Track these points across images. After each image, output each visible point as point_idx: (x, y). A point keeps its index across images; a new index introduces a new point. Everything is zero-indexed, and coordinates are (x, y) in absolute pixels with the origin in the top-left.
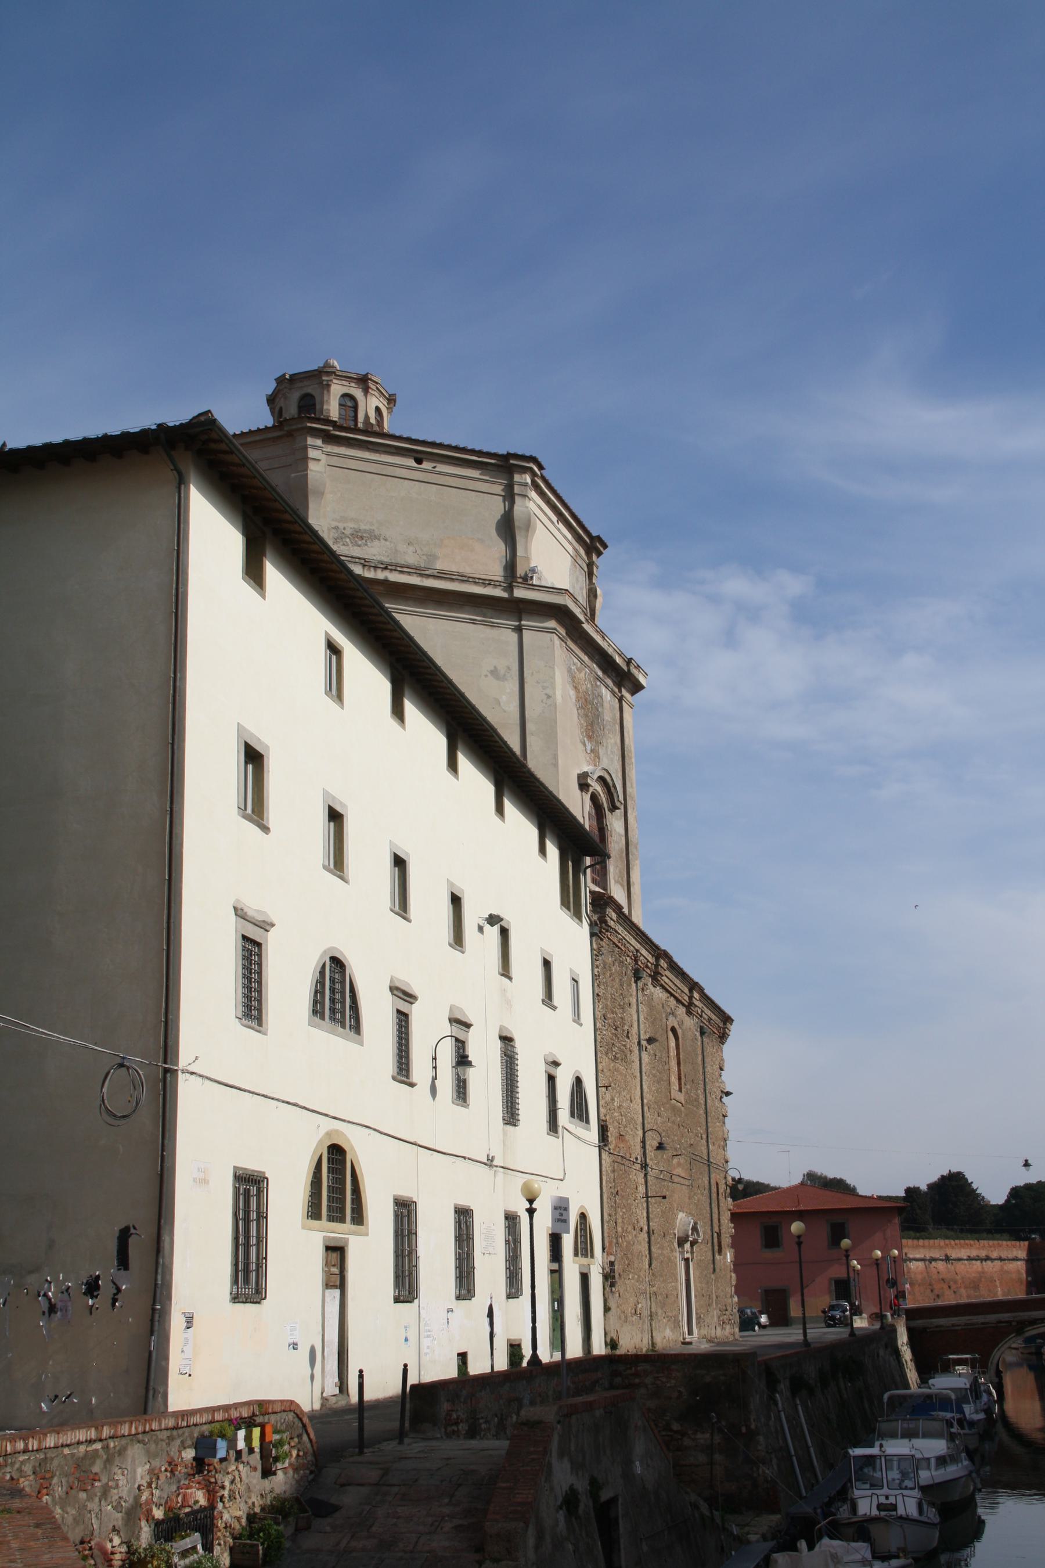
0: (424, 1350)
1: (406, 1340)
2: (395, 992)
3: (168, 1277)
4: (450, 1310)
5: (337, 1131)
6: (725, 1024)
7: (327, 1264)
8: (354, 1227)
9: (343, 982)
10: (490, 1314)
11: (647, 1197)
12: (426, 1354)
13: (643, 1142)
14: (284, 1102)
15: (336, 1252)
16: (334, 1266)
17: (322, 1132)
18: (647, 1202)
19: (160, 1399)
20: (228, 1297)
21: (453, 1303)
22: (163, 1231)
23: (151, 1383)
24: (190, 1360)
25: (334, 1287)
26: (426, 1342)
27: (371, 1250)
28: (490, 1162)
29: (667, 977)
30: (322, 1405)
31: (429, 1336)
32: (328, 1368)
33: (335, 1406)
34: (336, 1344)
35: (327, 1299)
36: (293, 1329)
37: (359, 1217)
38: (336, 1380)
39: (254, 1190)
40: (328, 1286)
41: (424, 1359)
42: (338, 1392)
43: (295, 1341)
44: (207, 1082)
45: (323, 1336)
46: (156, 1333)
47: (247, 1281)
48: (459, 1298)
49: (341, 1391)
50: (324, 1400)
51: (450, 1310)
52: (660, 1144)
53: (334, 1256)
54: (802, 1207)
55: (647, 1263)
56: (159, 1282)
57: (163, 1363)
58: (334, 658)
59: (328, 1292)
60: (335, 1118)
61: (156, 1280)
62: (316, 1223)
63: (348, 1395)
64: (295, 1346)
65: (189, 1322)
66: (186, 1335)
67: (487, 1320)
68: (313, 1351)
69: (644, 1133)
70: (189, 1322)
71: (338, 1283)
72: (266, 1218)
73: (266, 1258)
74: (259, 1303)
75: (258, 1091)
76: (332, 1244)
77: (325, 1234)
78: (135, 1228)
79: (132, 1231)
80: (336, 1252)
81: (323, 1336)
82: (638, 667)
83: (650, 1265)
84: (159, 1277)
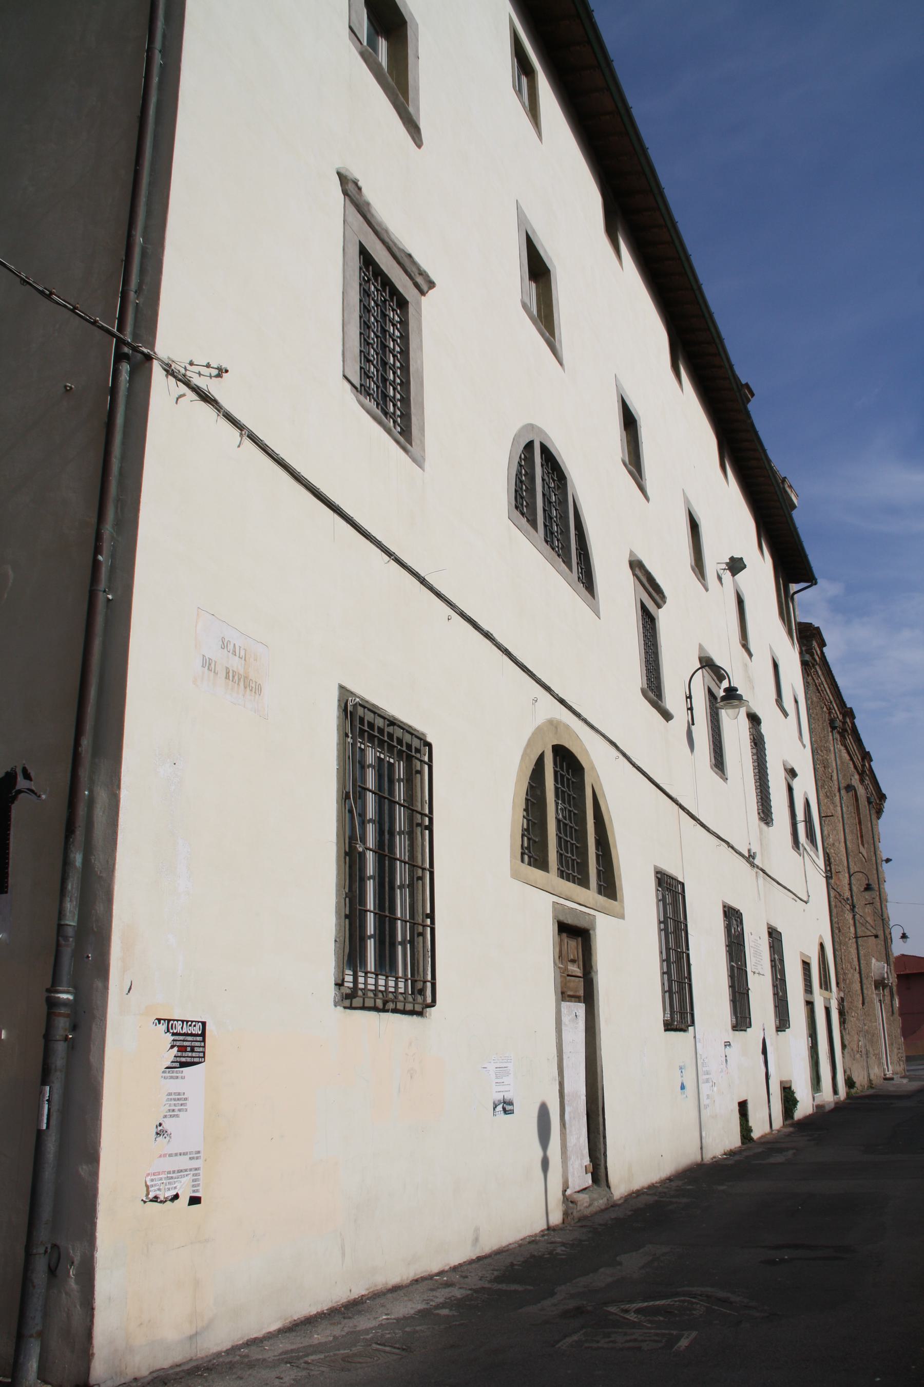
0: (704, 1101)
1: (683, 1087)
2: (638, 572)
3: (100, 908)
4: (728, 1044)
5: (567, 727)
6: (880, 801)
7: (561, 956)
8: (602, 899)
9: (564, 517)
10: (764, 1051)
11: (856, 937)
12: (706, 1107)
13: (850, 884)
14: (463, 615)
15: (575, 935)
16: (573, 961)
17: (540, 719)
18: (857, 942)
19: (72, 1284)
20: (330, 991)
21: (730, 1035)
22: (84, 774)
23: (43, 1234)
24: (195, 1155)
25: (575, 998)
26: (705, 1089)
27: (627, 945)
28: (750, 858)
29: (850, 740)
30: (566, 1214)
31: (707, 1081)
32: (572, 1140)
33: (587, 1212)
34: (583, 1098)
35: (565, 1019)
36: (502, 1071)
37: (609, 886)
38: (587, 1161)
39: (400, 770)
40: (565, 995)
41: (706, 1113)
42: (590, 1182)
43: (508, 1096)
44: (247, 443)
45: (561, 1084)
46: (58, 1078)
47: (386, 964)
48: (735, 1028)
49: (595, 1180)
50: (568, 1201)
51: (728, 1044)
52: (868, 885)
53: (573, 946)
54: (908, 972)
55: (861, 1002)
56: (71, 920)
57: (83, 1170)
58: (524, 80)
59: (565, 1005)
60: (562, 701)
61: (61, 914)
62: (536, 874)
63: (609, 1187)
64: (507, 1106)
65: (189, 1046)
66: (174, 1085)
67: (762, 1057)
68: (544, 1113)
69: (850, 877)
70: (189, 1046)
71: (581, 993)
72: (430, 828)
73: (432, 916)
74: (420, 1014)
75: (410, 563)
76: (569, 921)
77: (556, 899)
78: (27, 776)
79: (22, 783)
80: (575, 935)
81: (561, 1084)
82: (790, 487)
83: (863, 1004)
84: (70, 907)
